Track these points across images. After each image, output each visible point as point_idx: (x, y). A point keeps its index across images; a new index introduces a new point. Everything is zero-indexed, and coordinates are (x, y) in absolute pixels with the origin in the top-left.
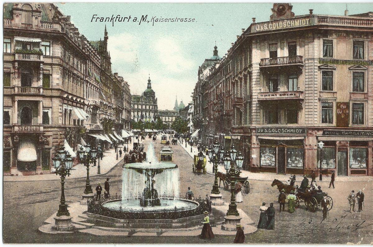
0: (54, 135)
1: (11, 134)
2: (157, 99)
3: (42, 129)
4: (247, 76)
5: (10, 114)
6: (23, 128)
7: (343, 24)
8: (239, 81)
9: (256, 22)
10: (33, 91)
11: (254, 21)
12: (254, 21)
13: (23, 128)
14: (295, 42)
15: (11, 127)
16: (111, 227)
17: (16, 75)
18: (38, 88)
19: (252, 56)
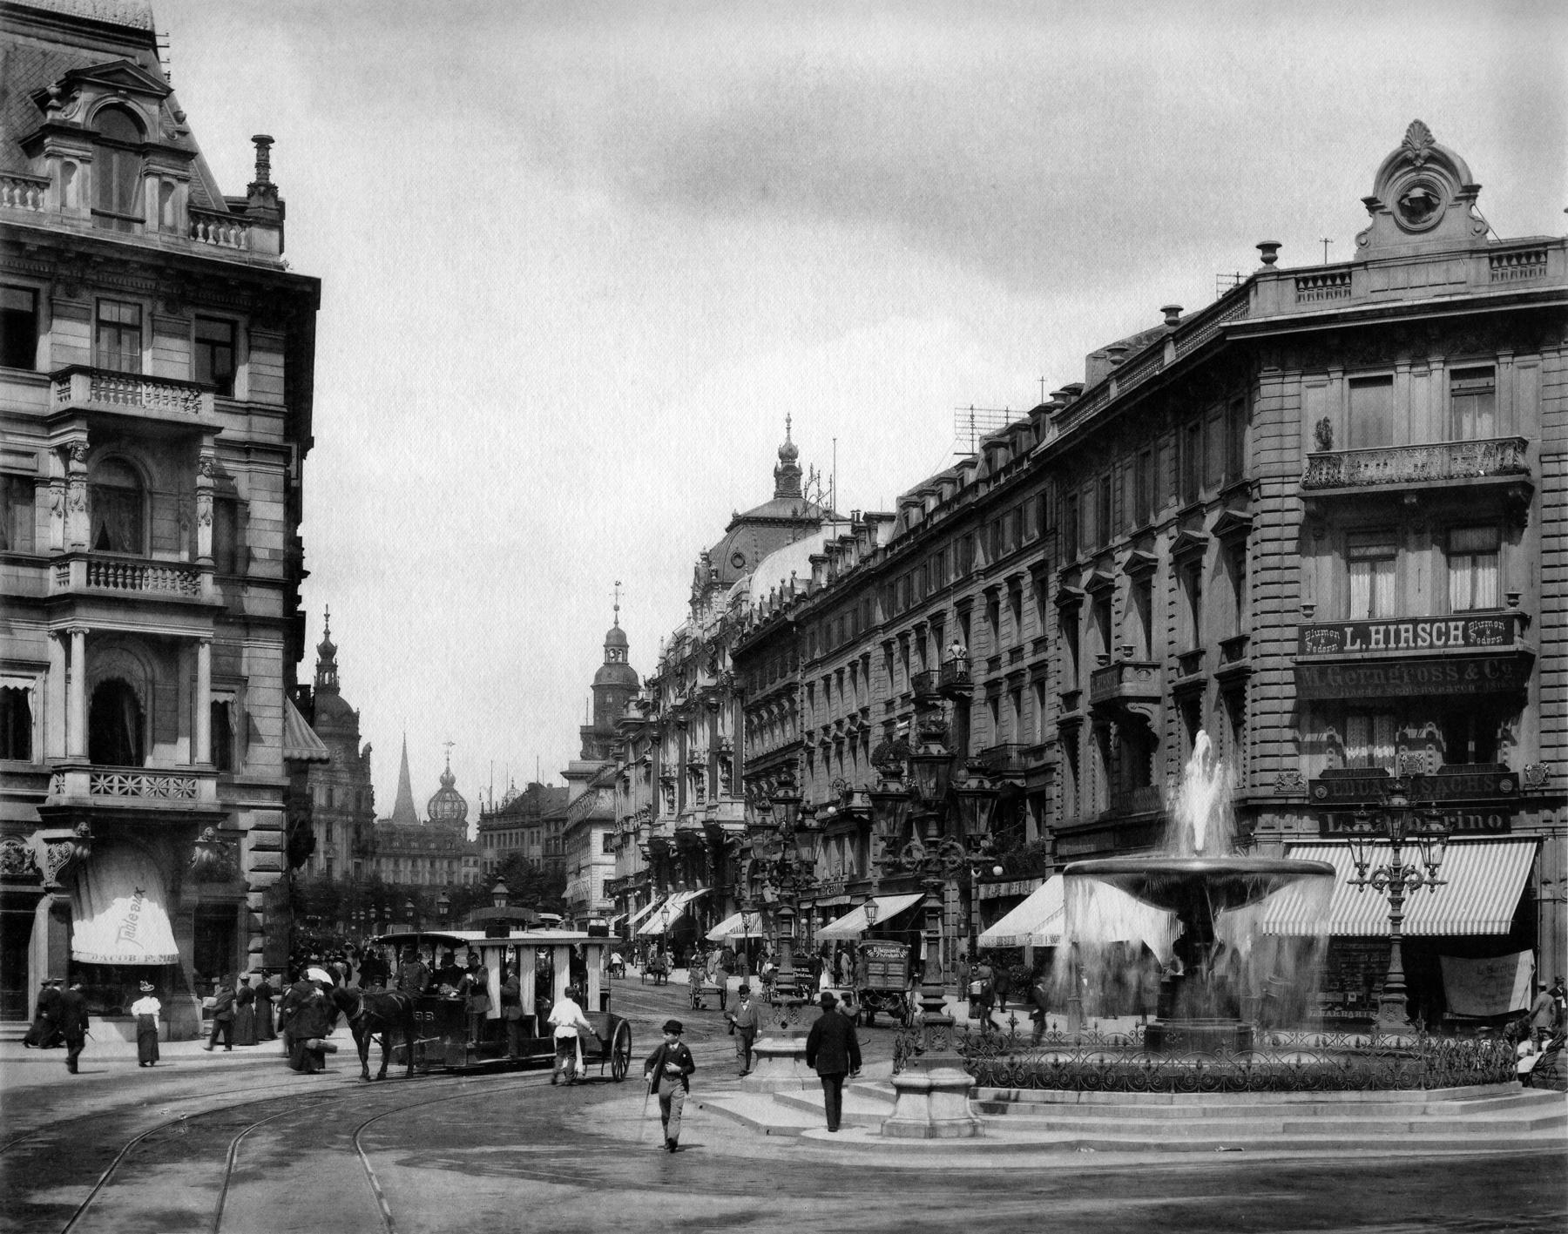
0: (258, 828)
1: (41, 810)
2: (368, 749)
3: (208, 792)
4: (1080, 603)
5: (34, 702)
6: (116, 779)
7: (1215, 584)
8: (847, 741)
9: (1282, 264)
10: (154, 586)
11: (1269, 261)
12: (1269, 261)
13: (116, 779)
14: (1489, 371)
15: (42, 778)
16: (1327, 498)
17: (79, 492)
18: (191, 570)
19: (1379, 1168)
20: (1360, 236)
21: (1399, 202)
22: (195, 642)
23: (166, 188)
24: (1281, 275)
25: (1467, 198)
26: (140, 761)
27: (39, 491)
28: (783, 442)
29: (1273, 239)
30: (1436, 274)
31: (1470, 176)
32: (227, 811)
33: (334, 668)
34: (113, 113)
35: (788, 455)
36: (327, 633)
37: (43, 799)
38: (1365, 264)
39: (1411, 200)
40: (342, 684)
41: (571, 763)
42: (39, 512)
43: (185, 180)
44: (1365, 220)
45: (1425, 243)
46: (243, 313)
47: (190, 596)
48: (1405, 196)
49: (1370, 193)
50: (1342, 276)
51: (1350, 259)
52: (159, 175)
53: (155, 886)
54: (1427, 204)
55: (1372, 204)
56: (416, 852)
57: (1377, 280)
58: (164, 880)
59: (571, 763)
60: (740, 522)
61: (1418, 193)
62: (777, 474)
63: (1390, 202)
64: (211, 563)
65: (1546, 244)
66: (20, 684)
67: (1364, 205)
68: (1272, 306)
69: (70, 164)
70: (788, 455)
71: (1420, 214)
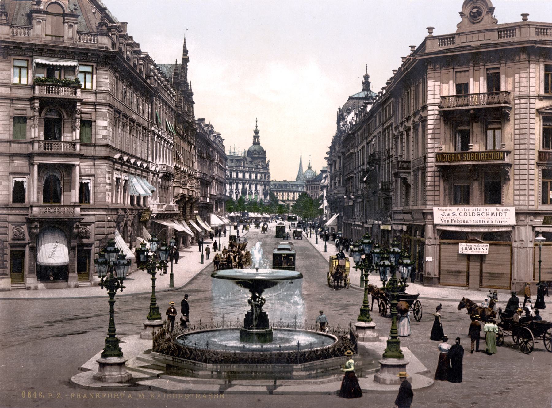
2: (269, 162)
5: (26, 185)
9: (435, 34)
10: (63, 148)
12: (430, 33)
20: (458, 24)
21: (470, 13)
22: (74, 166)
23: (71, 26)
24: (434, 38)
25: (490, 12)
26: (59, 201)
27: (28, 121)
28: (365, 73)
29: (432, 26)
30: (481, 36)
31: (491, 4)
32: (82, 217)
33: (259, 137)
34: (51, 5)
35: (366, 77)
36: (257, 127)
37: (27, 215)
38: (459, 34)
39: (473, 13)
40: (261, 142)
41: (323, 167)
42: (28, 127)
43: (77, 23)
44: (459, 20)
45: (478, 27)
46: (94, 63)
47: (73, 151)
48: (471, 12)
49: (461, 11)
50: (453, 38)
51: (454, 32)
52: (68, 23)
53: (63, 239)
54: (479, 13)
55: (461, 14)
56: (289, 190)
57: (464, 38)
58: (66, 237)
59: (323, 167)
60: (351, 98)
61: (475, 10)
62: (363, 83)
63: (467, 13)
64: (79, 141)
65: (515, 26)
66: (20, 180)
67: (459, 15)
68: (434, 47)
69: (39, 21)
70: (366, 77)
71: (476, 17)
